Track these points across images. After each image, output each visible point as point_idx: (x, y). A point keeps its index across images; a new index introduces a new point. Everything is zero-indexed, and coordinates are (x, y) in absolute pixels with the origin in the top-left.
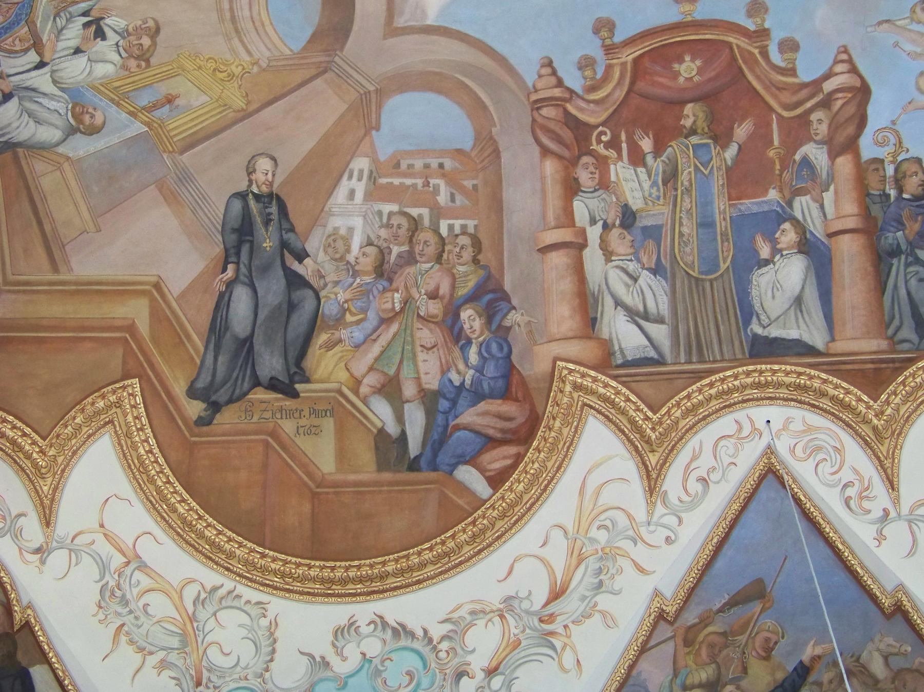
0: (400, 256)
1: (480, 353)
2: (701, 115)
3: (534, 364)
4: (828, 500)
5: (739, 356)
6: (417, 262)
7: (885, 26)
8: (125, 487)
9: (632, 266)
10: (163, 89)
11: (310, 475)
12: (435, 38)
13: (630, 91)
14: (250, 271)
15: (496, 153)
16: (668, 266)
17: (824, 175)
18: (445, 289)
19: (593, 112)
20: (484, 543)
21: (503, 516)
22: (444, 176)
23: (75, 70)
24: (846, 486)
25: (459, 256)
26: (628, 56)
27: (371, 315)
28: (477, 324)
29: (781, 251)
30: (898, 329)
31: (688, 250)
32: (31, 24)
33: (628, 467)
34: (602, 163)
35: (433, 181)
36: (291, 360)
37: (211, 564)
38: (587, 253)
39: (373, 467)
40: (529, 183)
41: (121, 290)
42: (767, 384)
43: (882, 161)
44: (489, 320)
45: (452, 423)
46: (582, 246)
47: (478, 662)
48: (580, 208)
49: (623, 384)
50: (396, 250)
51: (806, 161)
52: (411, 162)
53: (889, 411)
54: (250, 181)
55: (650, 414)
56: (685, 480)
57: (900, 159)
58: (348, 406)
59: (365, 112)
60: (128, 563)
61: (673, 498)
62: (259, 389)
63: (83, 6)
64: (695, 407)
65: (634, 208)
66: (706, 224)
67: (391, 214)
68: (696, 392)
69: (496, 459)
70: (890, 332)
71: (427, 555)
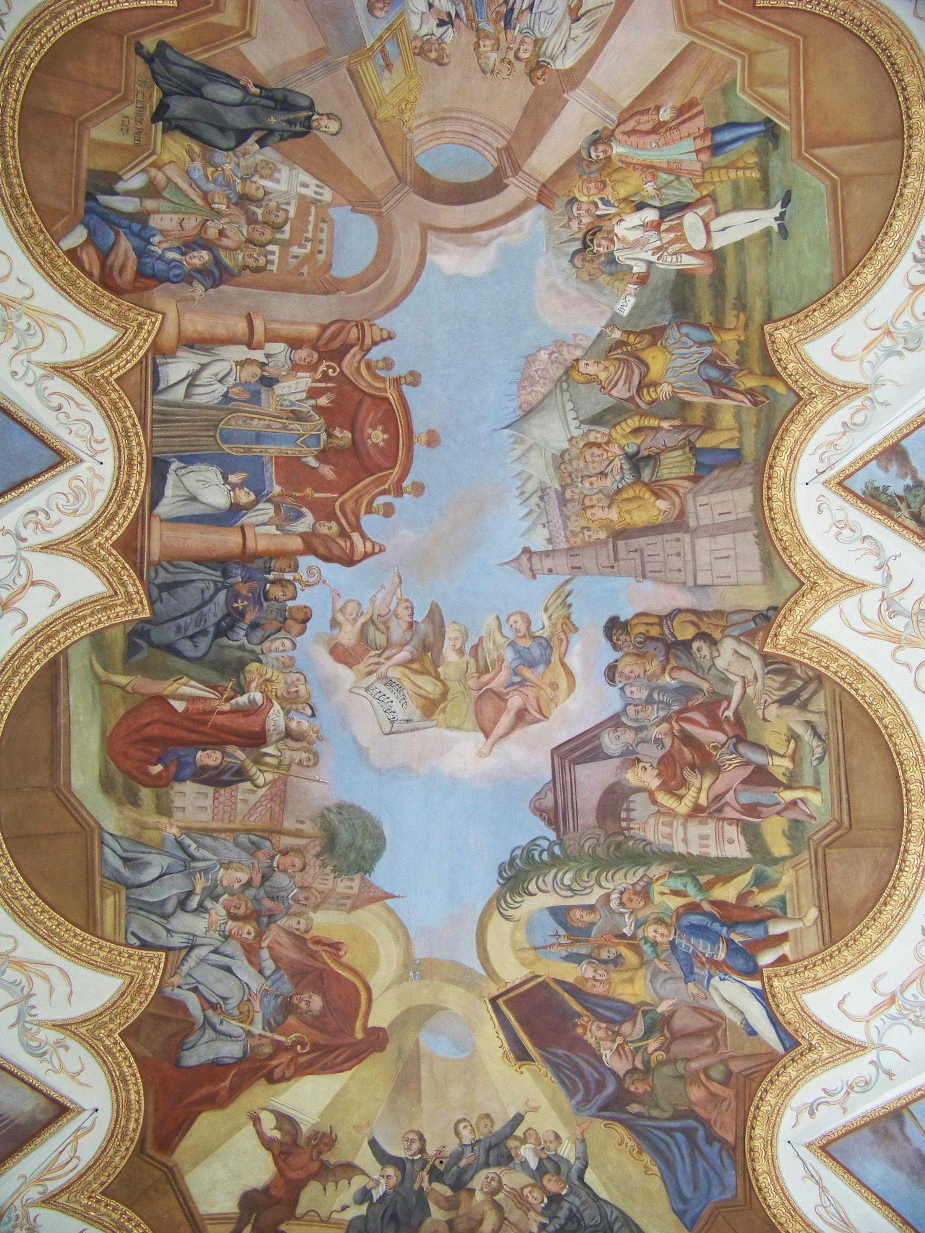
0: (254, 213)
1: (174, 260)
3: (163, 299)
4: (39, 497)
5: (155, 450)
6: (249, 225)
7: (397, 580)
9: (231, 380)
10: (397, 63)
11: (90, 119)
12: (417, 259)
13: (365, 393)
14: (254, 104)
15: (326, 292)
16: (229, 406)
17: (288, 528)
18: (225, 242)
19: (351, 365)
21: (44, 254)
22: (313, 253)
24: (47, 513)
25: (250, 256)
26: (391, 394)
27: (211, 186)
28: (197, 262)
29: (233, 490)
30: (166, 570)
31: (240, 422)
33: (74, 354)
34: (312, 368)
35: (309, 244)
36: (182, 123)
37: (24, 26)
38: (244, 348)
39: (92, 166)
40: (304, 313)
42: (131, 466)
43: (296, 571)
44: (198, 271)
48: (279, 348)
49: (140, 361)
50: (259, 211)
51: (301, 515)
53: (103, 552)
54: (322, 115)
55: (115, 376)
56: (61, 395)
57: (297, 584)
58: (141, 158)
59: (366, 202)
62: (161, 96)
63: (463, 14)
64: (117, 409)
66: (259, 438)
67: (287, 211)
68: (129, 412)
69: (90, 258)
70: (165, 564)
71: (18, 191)
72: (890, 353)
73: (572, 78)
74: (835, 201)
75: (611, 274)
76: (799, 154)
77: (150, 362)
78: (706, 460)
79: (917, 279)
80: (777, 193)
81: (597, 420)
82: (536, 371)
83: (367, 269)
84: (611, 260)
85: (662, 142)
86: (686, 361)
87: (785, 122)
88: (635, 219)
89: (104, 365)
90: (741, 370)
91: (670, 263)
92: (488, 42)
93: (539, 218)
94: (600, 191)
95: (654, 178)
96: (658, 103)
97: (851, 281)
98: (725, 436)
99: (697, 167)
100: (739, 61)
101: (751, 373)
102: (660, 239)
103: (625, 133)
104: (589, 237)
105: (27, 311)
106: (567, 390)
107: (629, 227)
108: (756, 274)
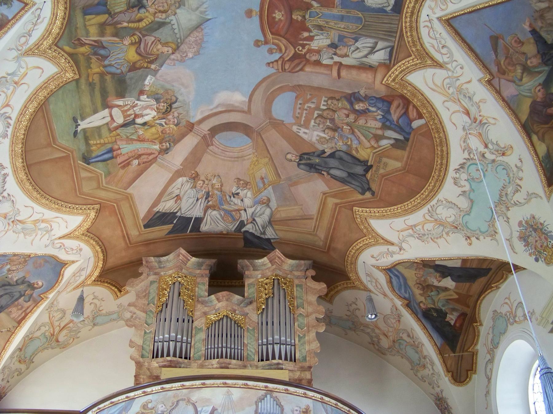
0: (331, 123)
1: (373, 107)
2: (298, 13)
3: (381, 90)
5: (398, 18)
8: (390, 221)
9: (353, 48)
10: (258, 179)
11: (400, 171)
12: (253, 99)
13: (283, 37)
15: (299, 86)
18: (346, 112)
20: (441, 128)
22: (304, 104)
23: (248, 202)
26: (270, 36)
27: (349, 136)
28: (361, 105)
31: (351, 27)
32: (232, 211)
33: (429, 72)
34: (310, 51)
35: (306, 107)
36: (359, 163)
38: (344, 63)
39: (404, 152)
40: (311, 77)
41: (323, 204)
45: (395, 123)
46: (341, 64)
47: (481, 148)
49: (397, 63)
50: (328, 124)
52: (297, 113)
55: (411, 58)
59: (277, 124)
60: (412, 229)
61: (446, 60)
62: (367, 175)
63: (228, 197)
64: (413, 42)
65: (330, 43)
66: (342, 18)
67: (315, 123)
68: (408, 39)
69: (413, 113)
72: (13, 74)
73: (178, 174)
74: (53, 136)
75: (157, 94)
76: (72, 153)
77: (392, 62)
78: (103, 8)
79: (7, 110)
80: (80, 136)
81: (162, 25)
82: (194, 48)
83: (278, 95)
84: (157, 100)
85: (136, 151)
86: (117, 57)
87: (80, 164)
88: (147, 119)
89: (416, 64)
90: (88, 55)
91: (129, 101)
92: (217, 187)
93: (193, 117)
94: (164, 130)
95: (139, 137)
96: (139, 167)
97: (39, 104)
98: (93, 22)
99: (118, 143)
100: (104, 185)
101: (83, 54)
102: (134, 111)
103: (154, 154)
104: (169, 110)
105: (448, 95)
106: (178, 38)
107: (150, 115)
108: (86, 100)
